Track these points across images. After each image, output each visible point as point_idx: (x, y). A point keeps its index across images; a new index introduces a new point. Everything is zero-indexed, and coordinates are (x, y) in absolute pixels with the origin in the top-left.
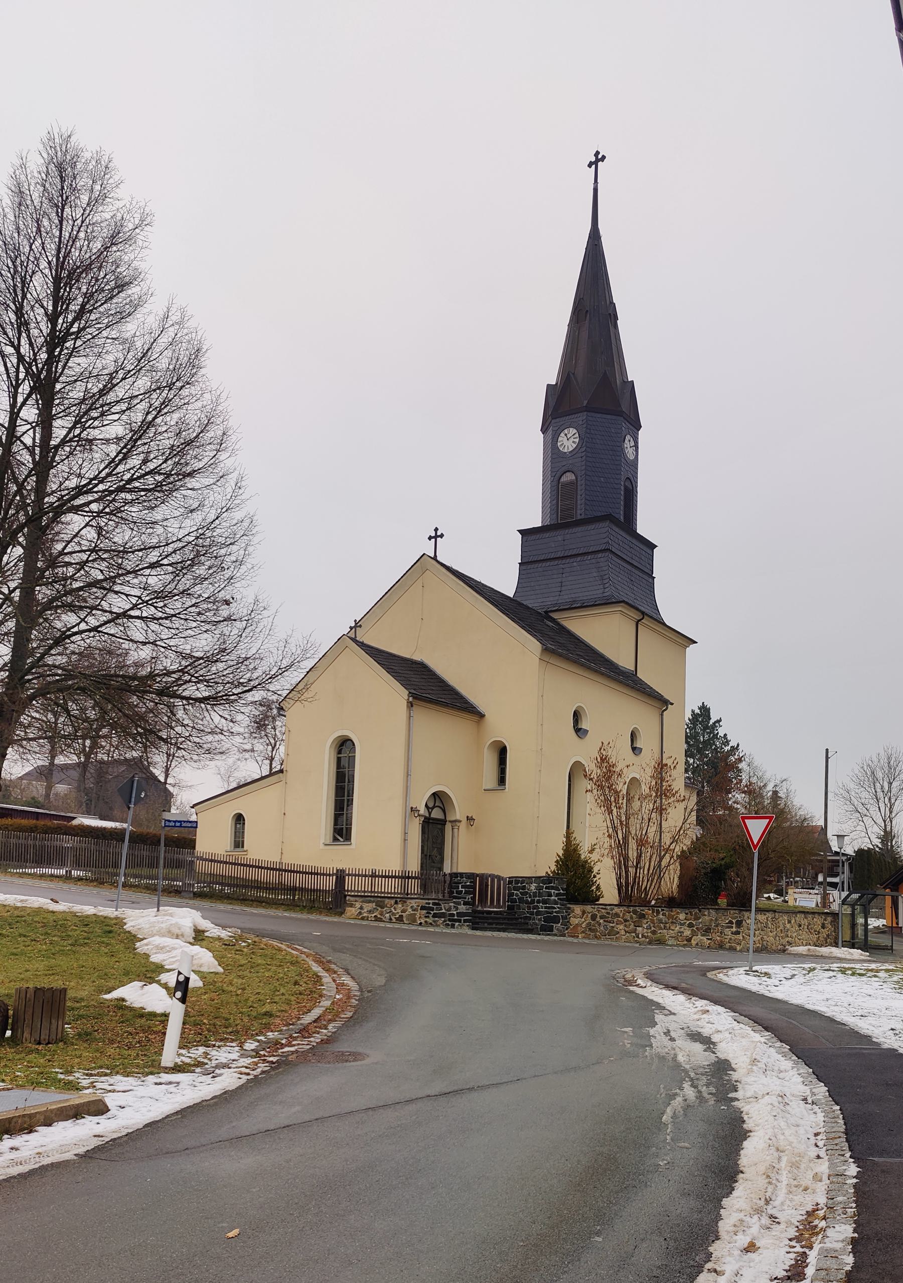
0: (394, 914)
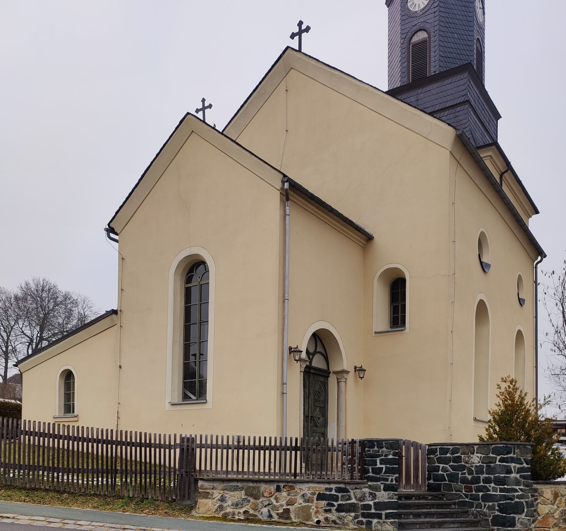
0: (275, 508)
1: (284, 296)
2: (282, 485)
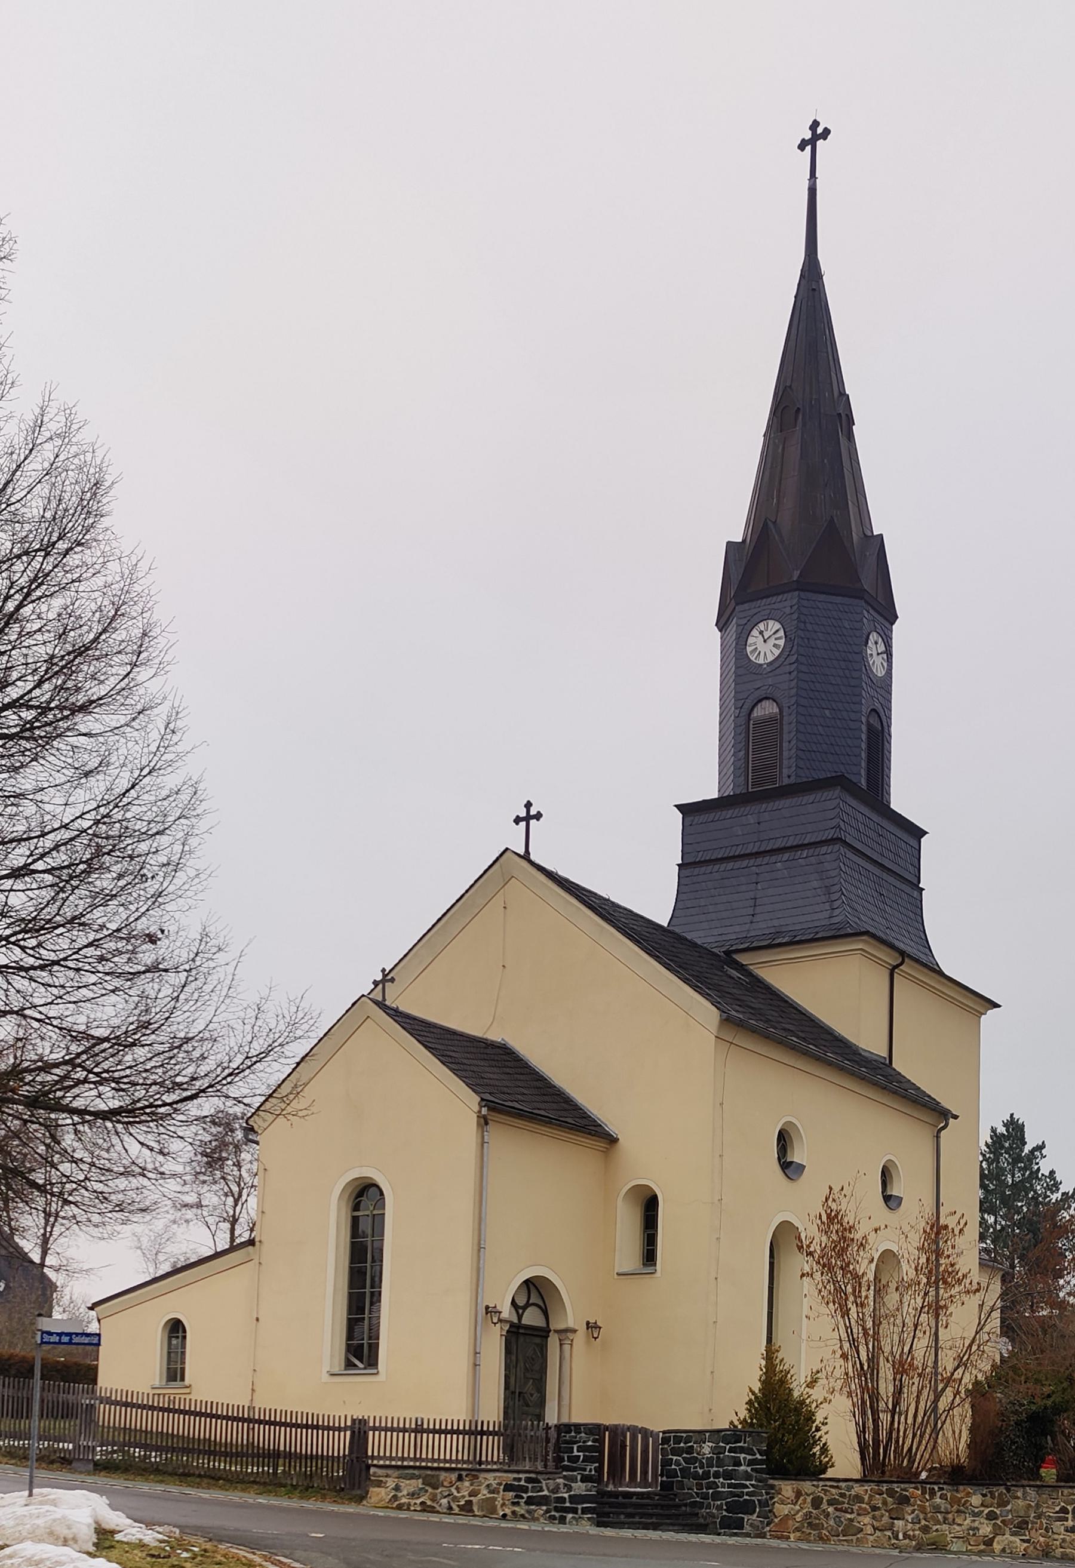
0: (456, 1499)
1: (479, 1243)
2: (464, 1473)
